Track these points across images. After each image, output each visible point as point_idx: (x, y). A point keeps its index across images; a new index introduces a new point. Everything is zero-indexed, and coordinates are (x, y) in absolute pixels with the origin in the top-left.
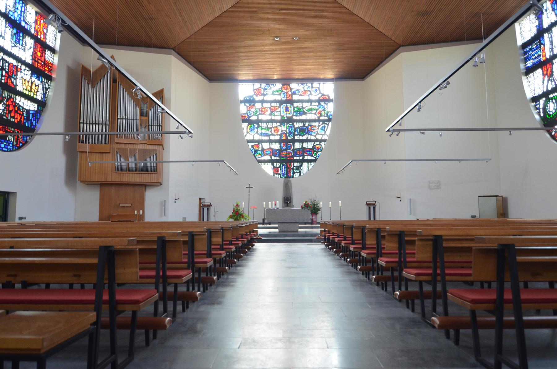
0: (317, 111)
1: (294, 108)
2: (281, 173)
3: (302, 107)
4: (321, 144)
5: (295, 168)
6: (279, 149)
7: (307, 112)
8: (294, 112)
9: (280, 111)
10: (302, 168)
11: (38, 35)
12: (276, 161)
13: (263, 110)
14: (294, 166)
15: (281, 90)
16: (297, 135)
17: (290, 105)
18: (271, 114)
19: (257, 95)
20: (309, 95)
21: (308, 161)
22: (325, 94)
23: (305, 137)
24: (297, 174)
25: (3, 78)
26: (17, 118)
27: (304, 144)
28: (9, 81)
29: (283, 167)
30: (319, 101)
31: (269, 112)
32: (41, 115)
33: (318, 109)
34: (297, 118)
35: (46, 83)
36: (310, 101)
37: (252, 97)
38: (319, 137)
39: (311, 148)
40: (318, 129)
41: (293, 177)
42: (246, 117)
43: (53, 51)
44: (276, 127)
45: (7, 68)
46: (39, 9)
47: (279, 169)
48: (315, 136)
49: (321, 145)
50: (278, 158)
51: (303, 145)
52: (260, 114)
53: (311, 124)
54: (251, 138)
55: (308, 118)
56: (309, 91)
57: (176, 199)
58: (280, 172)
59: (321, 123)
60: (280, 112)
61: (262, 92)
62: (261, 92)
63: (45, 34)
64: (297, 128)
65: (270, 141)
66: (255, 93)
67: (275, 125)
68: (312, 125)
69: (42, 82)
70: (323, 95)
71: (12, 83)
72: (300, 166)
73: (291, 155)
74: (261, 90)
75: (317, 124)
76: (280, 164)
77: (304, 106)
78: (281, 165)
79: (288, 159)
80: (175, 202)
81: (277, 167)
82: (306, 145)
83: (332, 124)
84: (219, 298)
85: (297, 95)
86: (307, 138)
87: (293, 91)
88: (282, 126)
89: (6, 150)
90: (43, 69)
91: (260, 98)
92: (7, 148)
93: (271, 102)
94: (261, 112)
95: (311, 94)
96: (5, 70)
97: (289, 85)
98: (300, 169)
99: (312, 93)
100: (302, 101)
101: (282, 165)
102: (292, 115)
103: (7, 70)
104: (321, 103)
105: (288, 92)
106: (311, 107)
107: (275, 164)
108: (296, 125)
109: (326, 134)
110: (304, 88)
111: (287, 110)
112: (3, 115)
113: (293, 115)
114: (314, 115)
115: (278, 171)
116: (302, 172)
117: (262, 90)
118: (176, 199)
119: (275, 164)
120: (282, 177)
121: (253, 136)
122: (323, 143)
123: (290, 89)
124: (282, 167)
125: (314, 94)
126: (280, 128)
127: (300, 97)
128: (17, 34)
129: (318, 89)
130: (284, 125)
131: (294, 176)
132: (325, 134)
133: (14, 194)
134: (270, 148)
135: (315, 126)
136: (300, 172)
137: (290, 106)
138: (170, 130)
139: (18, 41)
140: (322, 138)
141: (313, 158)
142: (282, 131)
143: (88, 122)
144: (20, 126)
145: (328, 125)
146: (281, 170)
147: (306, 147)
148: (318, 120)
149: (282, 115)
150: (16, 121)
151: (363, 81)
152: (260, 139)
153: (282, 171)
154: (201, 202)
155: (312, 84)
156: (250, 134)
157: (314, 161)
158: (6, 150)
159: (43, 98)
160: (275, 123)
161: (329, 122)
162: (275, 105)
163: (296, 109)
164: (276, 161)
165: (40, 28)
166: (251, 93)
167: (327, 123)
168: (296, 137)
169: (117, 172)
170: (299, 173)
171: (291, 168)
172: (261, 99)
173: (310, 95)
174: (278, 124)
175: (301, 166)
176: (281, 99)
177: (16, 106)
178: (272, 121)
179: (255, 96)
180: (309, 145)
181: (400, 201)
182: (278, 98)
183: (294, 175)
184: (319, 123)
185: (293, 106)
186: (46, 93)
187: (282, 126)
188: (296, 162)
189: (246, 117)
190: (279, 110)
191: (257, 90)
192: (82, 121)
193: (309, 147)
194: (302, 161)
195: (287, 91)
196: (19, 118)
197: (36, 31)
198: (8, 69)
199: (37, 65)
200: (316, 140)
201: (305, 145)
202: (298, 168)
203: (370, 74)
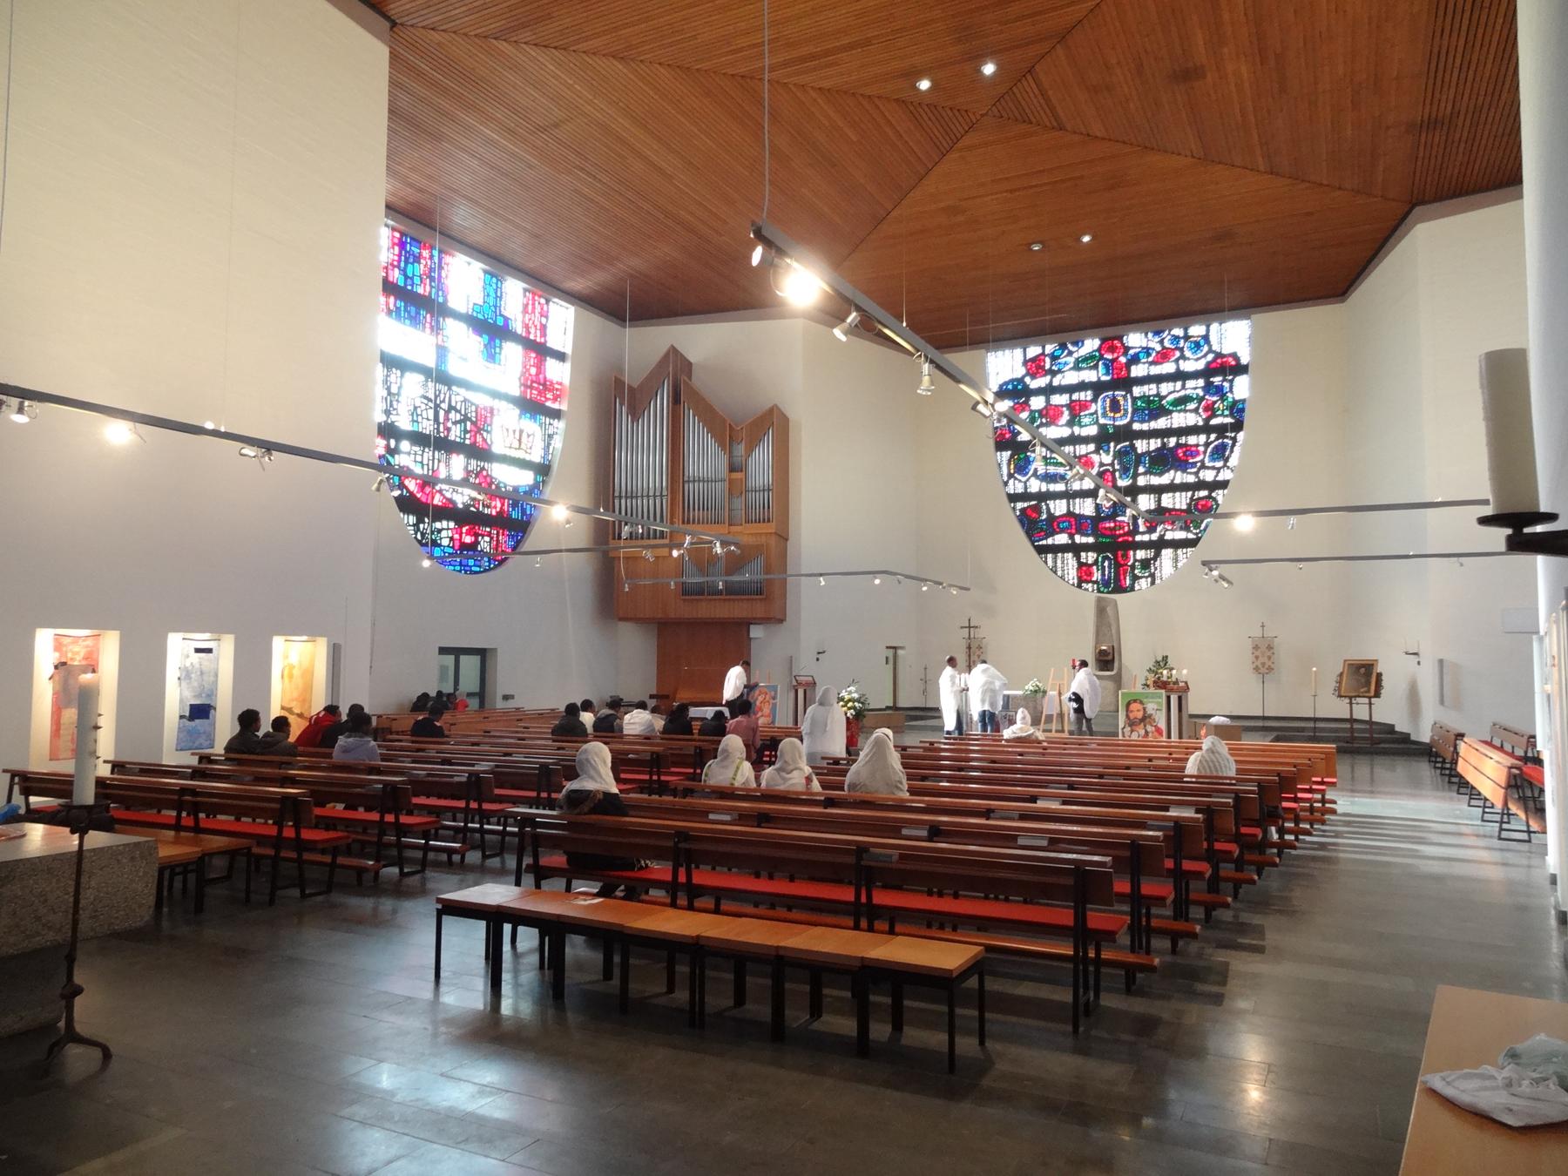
0: (1200, 403)
1: (1134, 399)
2: (1100, 578)
3: (1158, 395)
4: (1214, 495)
5: (1137, 564)
6: (1094, 514)
7: (1171, 408)
8: (1135, 411)
9: (1096, 412)
10: (1158, 563)
11: (529, 333)
12: (1087, 548)
13: (1051, 412)
14: (1136, 560)
15: (1097, 354)
16: (1145, 474)
17: (1124, 393)
18: (1070, 424)
19: (1034, 376)
20: (1177, 361)
21: (1177, 545)
22: (1225, 352)
23: (1165, 479)
24: (1144, 579)
25: (468, 436)
26: (495, 507)
27: (1164, 496)
28: (479, 439)
29: (1106, 564)
30: (1207, 373)
31: (1066, 416)
32: (541, 491)
33: (1202, 399)
34: (1145, 427)
35: (550, 424)
36: (1180, 376)
37: (1021, 380)
38: (1208, 476)
39: (1184, 507)
40: (1205, 453)
41: (1132, 589)
42: (1007, 436)
43: (561, 357)
44: (1086, 455)
45: (474, 414)
46: (526, 283)
47: (1095, 567)
48: (1196, 474)
49: (1215, 499)
50: (1091, 540)
51: (1159, 501)
52: (1042, 425)
53: (1183, 440)
54: (1020, 489)
55: (1175, 426)
56: (1177, 349)
57: (819, 653)
58: (1097, 576)
59: (1213, 436)
60: (1095, 416)
61: (1047, 366)
62: (1044, 366)
63: (543, 328)
64: (1143, 454)
65: (1069, 495)
66: (1028, 370)
67: (1082, 449)
68: (1186, 445)
69: (541, 425)
70: (1219, 355)
71: (484, 440)
72: (1151, 559)
73: (1126, 529)
74: (1044, 361)
75: (1202, 438)
76: (1095, 555)
77: (1164, 393)
78: (1100, 559)
79: (1120, 539)
80: (818, 659)
81: (1090, 562)
82: (1171, 500)
83: (1245, 436)
84: (1263, 904)
85: (1144, 363)
86: (1172, 481)
87: (1131, 352)
88: (1101, 452)
89: (478, 569)
90: (543, 399)
91: (1041, 382)
92: (480, 567)
93: (1070, 389)
94: (1044, 420)
95: (1183, 357)
96: (470, 419)
97: (1120, 338)
98: (1152, 568)
99: (1188, 353)
100: (1159, 379)
101: (1103, 557)
102: (1128, 419)
103: (474, 419)
104: (1211, 379)
105: (1117, 358)
106: (1182, 393)
107: (1083, 554)
108: (1141, 446)
109: (1228, 468)
110: (1161, 342)
111: (1115, 406)
112: (470, 505)
113: (1132, 421)
114: (1193, 415)
115: (1091, 574)
116: (1158, 574)
117: (1048, 360)
118: (819, 653)
119: (1083, 554)
120: (1102, 589)
121: (1025, 483)
122: (1220, 492)
123: (1122, 350)
124: (1103, 562)
125: (1191, 356)
126: (1095, 458)
127: (1152, 367)
128: (492, 339)
129: (1202, 342)
130: (1106, 448)
131: (1137, 587)
132: (1225, 466)
133: (494, 650)
134: (1070, 514)
135: (1197, 445)
136: (1153, 576)
137: (1125, 397)
138: (1254, 328)
139: (491, 357)
140: (1217, 479)
141: (1191, 536)
142: (1102, 464)
143: (623, 494)
144: (499, 521)
145: (1234, 440)
146: (1100, 572)
147: (1171, 506)
148: (1206, 429)
149: (1102, 421)
150: (494, 513)
151: (1343, 301)
152: (1044, 489)
153: (1103, 574)
154: (794, 674)
155: (1186, 330)
156: (1016, 479)
157: (1191, 543)
158: (478, 569)
159: (544, 458)
160: (1082, 446)
161: (1238, 432)
162: (1083, 398)
163: (1139, 403)
164: (1087, 548)
165: (533, 318)
166: (1020, 371)
167: (1233, 435)
168: (1141, 481)
169: (684, 597)
170: (1149, 579)
171: (1126, 565)
172: (1043, 385)
173: (1181, 362)
174: (1092, 447)
175: (1155, 559)
176: (1099, 378)
177: (493, 483)
178: (1074, 440)
179: (1027, 380)
180: (1178, 500)
181: (1419, 663)
182: (1090, 376)
183: (1136, 585)
184: (1208, 438)
185: (1132, 395)
186: (549, 444)
187: (1101, 452)
188: (1142, 549)
189: (1007, 436)
190: (1092, 409)
191: (1033, 360)
192: (617, 494)
193: (1177, 507)
194: (1160, 545)
195: (1116, 355)
196: (499, 505)
197: (527, 327)
198: (476, 417)
199: (531, 393)
200: (1201, 485)
201: (1167, 500)
202: (1146, 564)
203: (1357, 283)
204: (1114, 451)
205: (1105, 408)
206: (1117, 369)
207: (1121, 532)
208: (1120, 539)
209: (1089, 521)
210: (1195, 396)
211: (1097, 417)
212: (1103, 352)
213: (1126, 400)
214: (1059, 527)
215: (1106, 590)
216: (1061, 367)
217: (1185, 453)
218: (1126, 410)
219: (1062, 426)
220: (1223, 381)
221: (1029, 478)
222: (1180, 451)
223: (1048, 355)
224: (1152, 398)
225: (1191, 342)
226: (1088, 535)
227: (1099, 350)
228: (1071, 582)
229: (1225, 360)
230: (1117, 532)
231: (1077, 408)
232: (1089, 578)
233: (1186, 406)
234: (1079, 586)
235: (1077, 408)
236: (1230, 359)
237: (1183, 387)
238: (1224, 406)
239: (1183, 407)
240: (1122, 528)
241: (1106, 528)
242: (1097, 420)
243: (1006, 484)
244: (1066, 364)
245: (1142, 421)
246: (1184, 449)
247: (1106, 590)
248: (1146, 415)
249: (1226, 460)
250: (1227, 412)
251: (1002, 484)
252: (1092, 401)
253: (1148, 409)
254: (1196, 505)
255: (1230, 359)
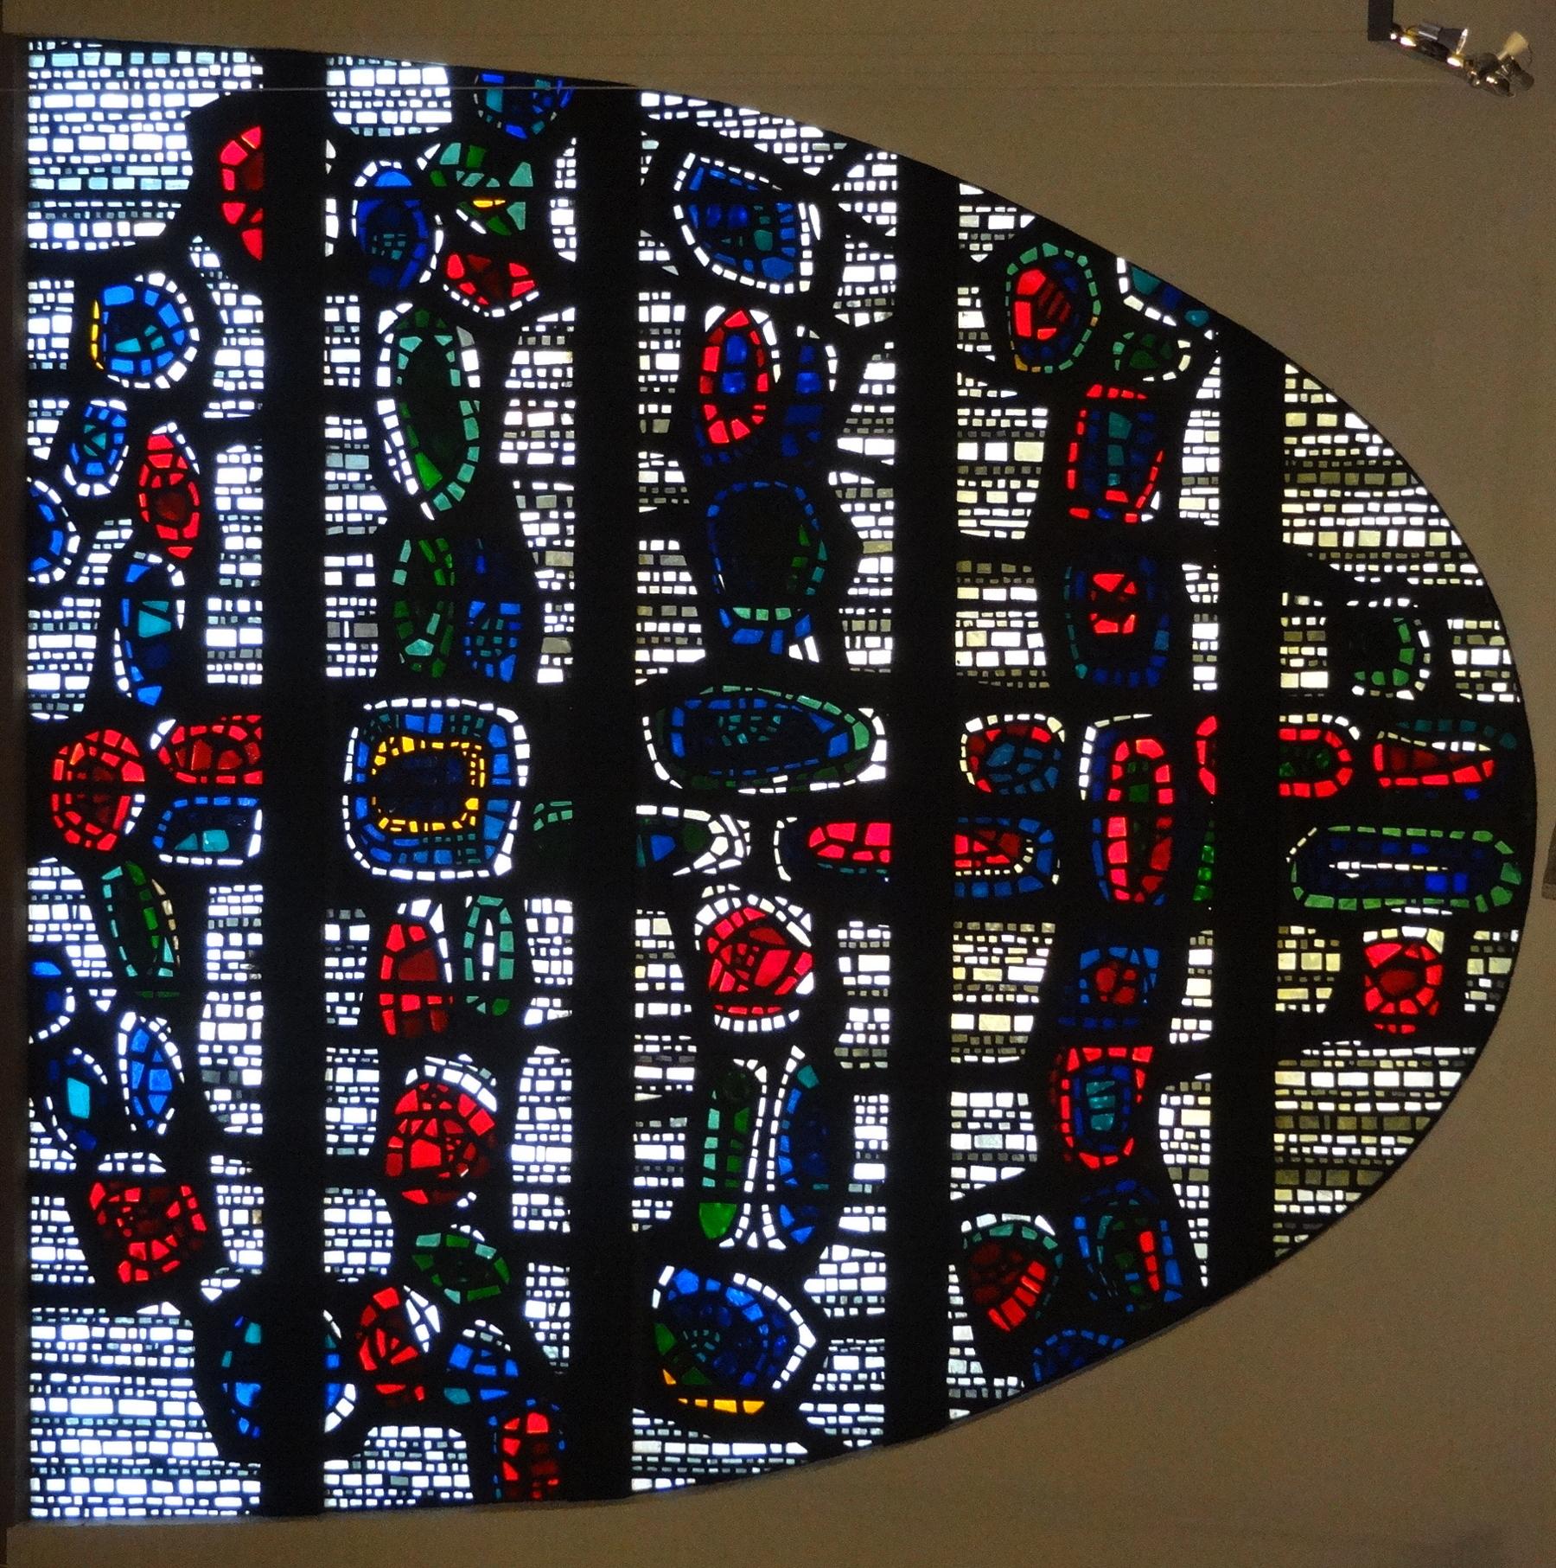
7: (466, 473)
13: (426, 1155)
33: (429, 299)
40: (740, 299)
64: (713, 638)
78: (1323, 902)
79: (1209, 782)
105: (147, 759)
120: (1501, 896)
129: (119, 295)
142: (754, 875)
145: (680, 136)
146: (1396, 905)
153: (1414, 888)
184: (654, 277)
189: (537, 1425)
204: (683, 802)
205: (429, 843)
206: (213, 772)
207: (1164, 775)
208: (1209, 782)
209: (1088, 958)
210: (411, 343)
211: (476, 887)
212: (107, 843)
213: (395, 725)
214: (1112, 1140)
215: (1511, 875)
216: (159, 1080)
217: (731, 408)
218: (454, 723)
219: (508, 1096)
220: (345, 195)
221: (802, 1302)
222: (717, 433)
223: (87, 1159)
224: (400, 577)
225: (108, 354)
226: (1179, 973)
227: (87, 865)
228: (1449, 1079)
229: (229, 181)
230: (1166, 797)
231: (411, 1003)
232: (1433, 975)
233: (465, 391)
234: (1477, 1030)
235: (411, 1003)
236: (232, 153)
237: (359, 403)
238: (481, 191)
239: (466, 407)
240: (1142, 769)
241: (1138, 867)
242: (493, 885)
243: (825, 1447)
244: (148, 1055)
245: (531, 642)
246: (710, 411)
247: (1511, 875)
248: (491, 612)
249: (793, 183)
250: (523, 176)
251: (831, 1472)
252: (382, 920)
253: (457, 597)
254: (1033, 351)
255: (232, 153)
